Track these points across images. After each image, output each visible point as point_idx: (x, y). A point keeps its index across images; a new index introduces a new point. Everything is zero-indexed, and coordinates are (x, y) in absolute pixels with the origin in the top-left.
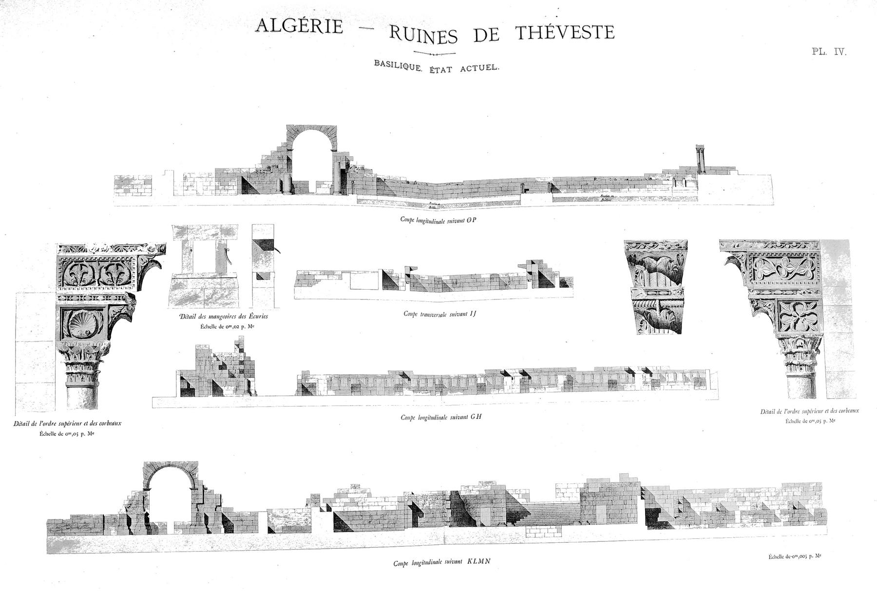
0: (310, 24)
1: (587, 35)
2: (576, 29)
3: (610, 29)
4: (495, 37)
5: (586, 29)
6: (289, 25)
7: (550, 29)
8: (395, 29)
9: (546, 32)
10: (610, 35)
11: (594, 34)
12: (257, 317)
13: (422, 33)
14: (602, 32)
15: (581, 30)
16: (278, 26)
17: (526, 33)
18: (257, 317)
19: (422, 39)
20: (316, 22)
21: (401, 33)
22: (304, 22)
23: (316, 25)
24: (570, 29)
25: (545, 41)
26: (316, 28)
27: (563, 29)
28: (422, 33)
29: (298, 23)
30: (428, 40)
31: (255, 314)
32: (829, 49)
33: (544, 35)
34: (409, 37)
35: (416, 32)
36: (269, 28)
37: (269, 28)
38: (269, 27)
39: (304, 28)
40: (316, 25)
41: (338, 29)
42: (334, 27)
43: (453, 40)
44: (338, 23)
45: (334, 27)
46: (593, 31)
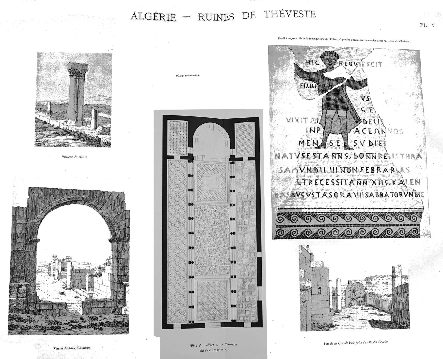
0: (159, 16)
1: (302, 15)
2: (296, 12)
3: (313, 12)
4: (253, 16)
5: (301, 12)
6: (148, 16)
7: (282, 12)
8: (201, 15)
9: (280, 14)
10: (313, 16)
11: (305, 15)
12: (382, 342)
13: (216, 16)
14: (309, 14)
15: (298, 13)
16: (142, 16)
17: (270, 14)
18: (382, 342)
19: (216, 19)
20: (162, 15)
21: (204, 17)
22: (156, 15)
23: (162, 17)
24: (292, 12)
25: (279, 18)
26: (162, 18)
27: (289, 12)
28: (216, 16)
29: (153, 15)
30: (219, 19)
31: (381, 341)
32: (428, 24)
33: (279, 15)
34: (209, 18)
35: (213, 16)
36: (138, 17)
37: (138, 17)
38: (138, 17)
39: (156, 18)
40: (162, 17)
41: (173, 19)
42: (171, 18)
43: (232, 18)
44: (173, 16)
45: (171, 18)
46: (305, 13)
